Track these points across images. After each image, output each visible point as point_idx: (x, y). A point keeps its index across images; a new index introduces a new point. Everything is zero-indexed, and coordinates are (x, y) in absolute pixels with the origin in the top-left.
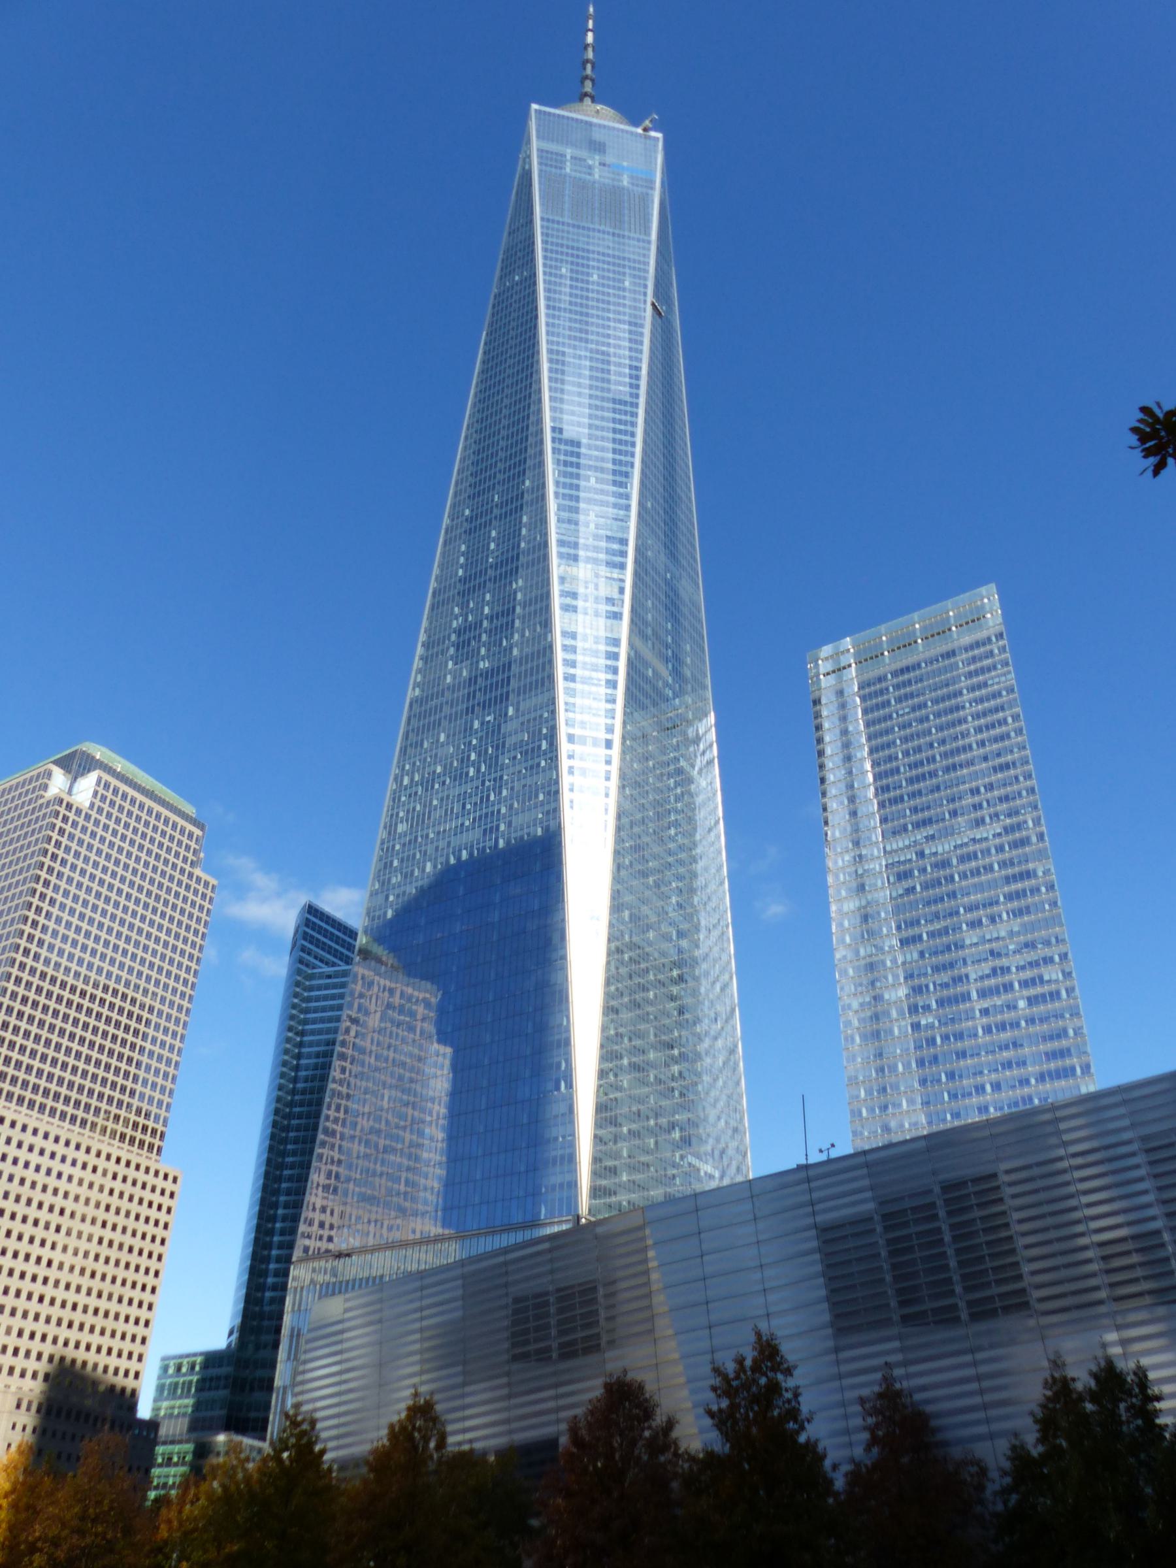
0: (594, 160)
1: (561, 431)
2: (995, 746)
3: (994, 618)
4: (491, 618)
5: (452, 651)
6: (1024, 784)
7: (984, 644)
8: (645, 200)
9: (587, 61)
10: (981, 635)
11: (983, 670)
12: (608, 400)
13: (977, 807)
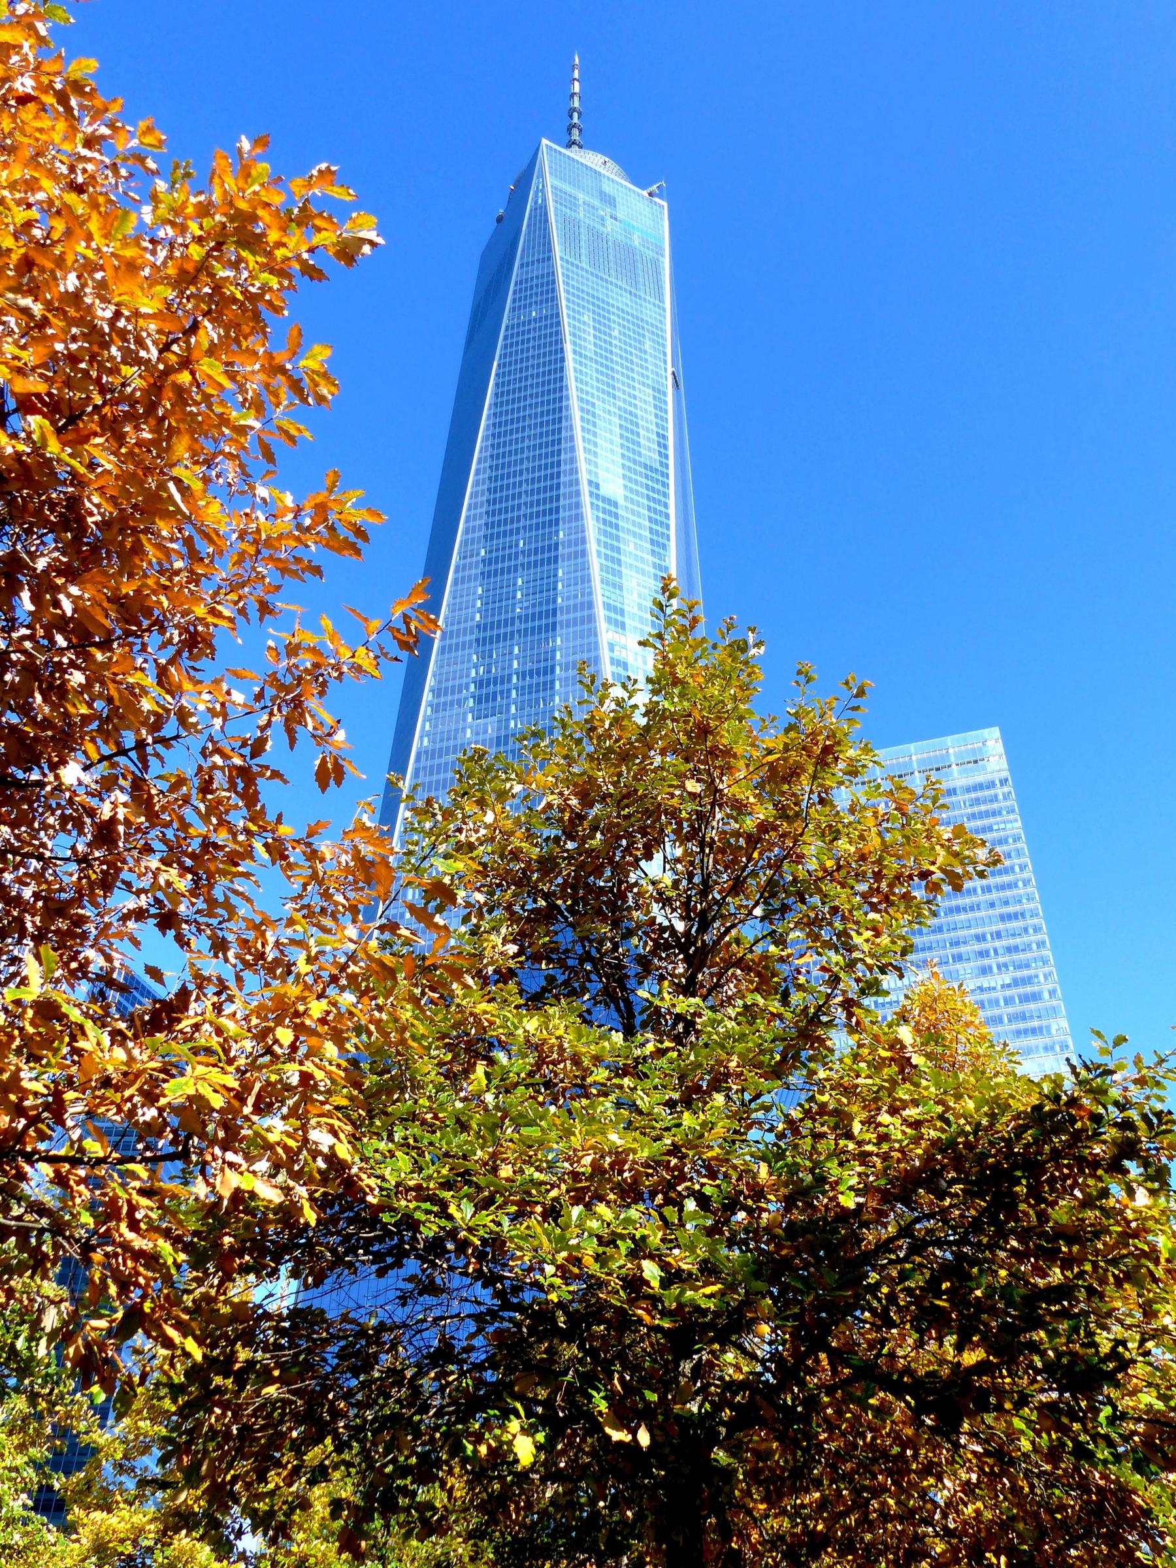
0: (605, 211)
1: (597, 486)
2: (1001, 894)
3: (996, 763)
4: (522, 675)
5: (471, 702)
6: (1034, 938)
7: (988, 787)
8: (656, 264)
9: (574, 110)
10: (980, 778)
11: (987, 814)
12: (640, 464)
13: (983, 954)
